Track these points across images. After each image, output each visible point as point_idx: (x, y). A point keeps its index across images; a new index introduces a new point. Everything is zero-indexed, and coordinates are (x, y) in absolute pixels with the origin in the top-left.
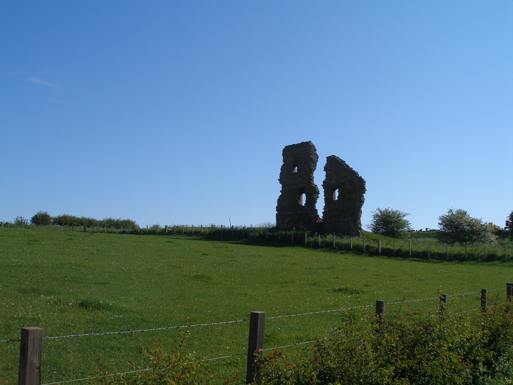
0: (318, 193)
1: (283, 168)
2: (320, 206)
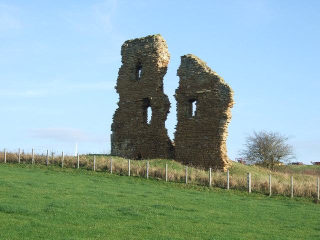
0: (168, 105)
1: (121, 72)
2: (171, 124)
